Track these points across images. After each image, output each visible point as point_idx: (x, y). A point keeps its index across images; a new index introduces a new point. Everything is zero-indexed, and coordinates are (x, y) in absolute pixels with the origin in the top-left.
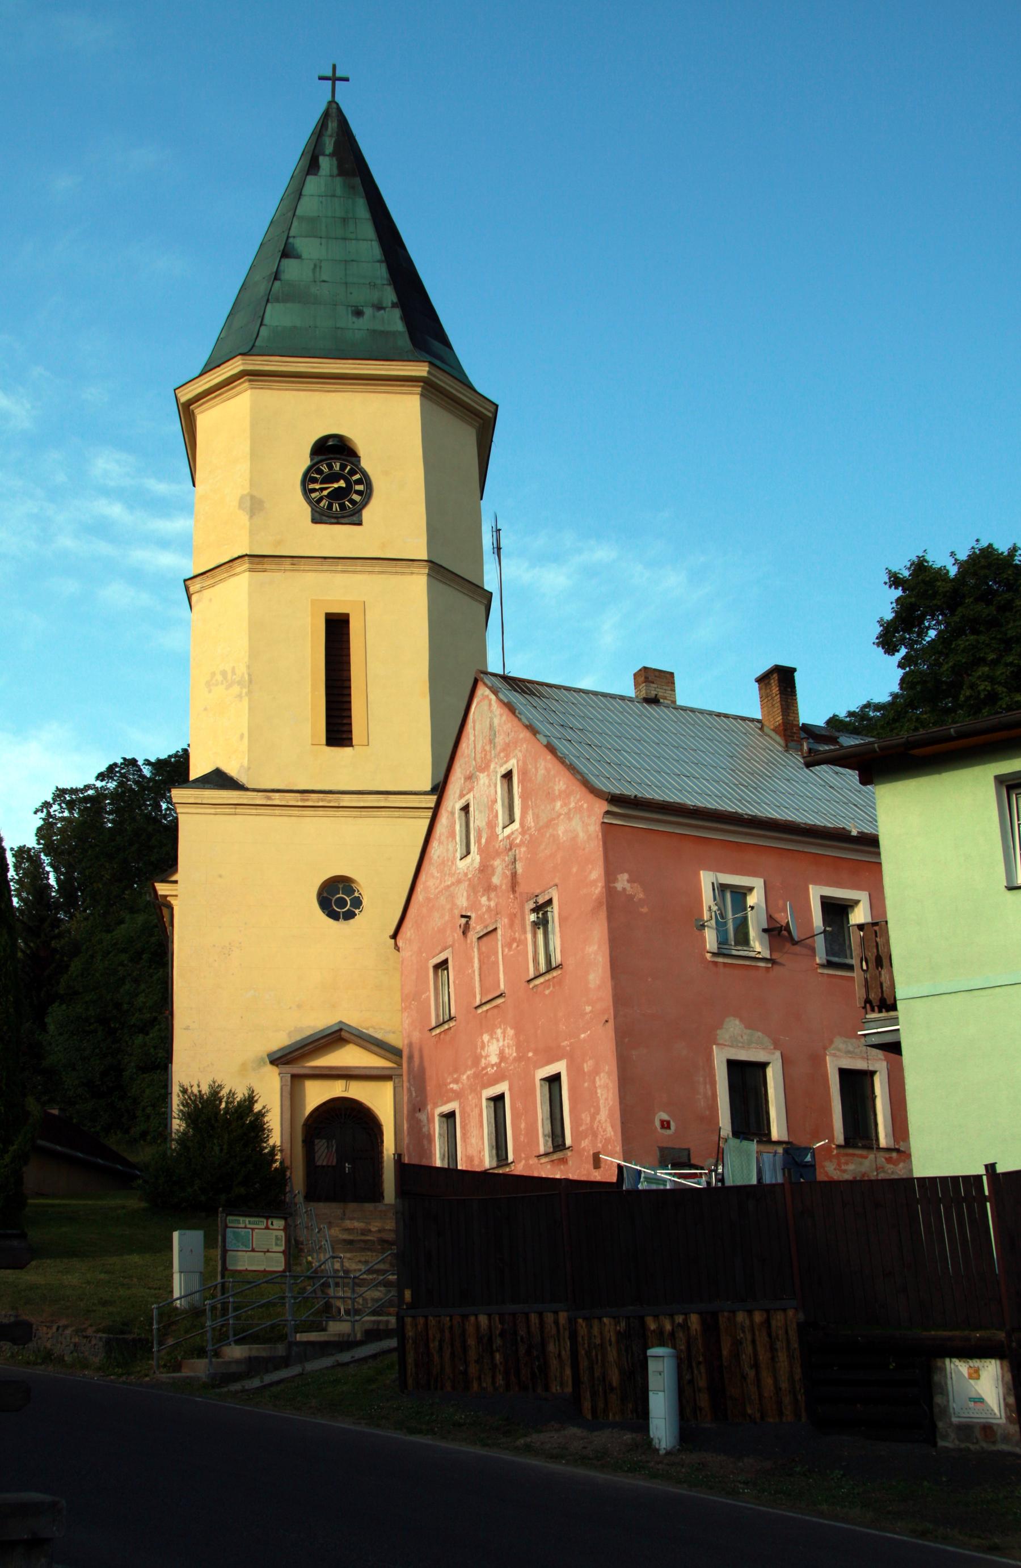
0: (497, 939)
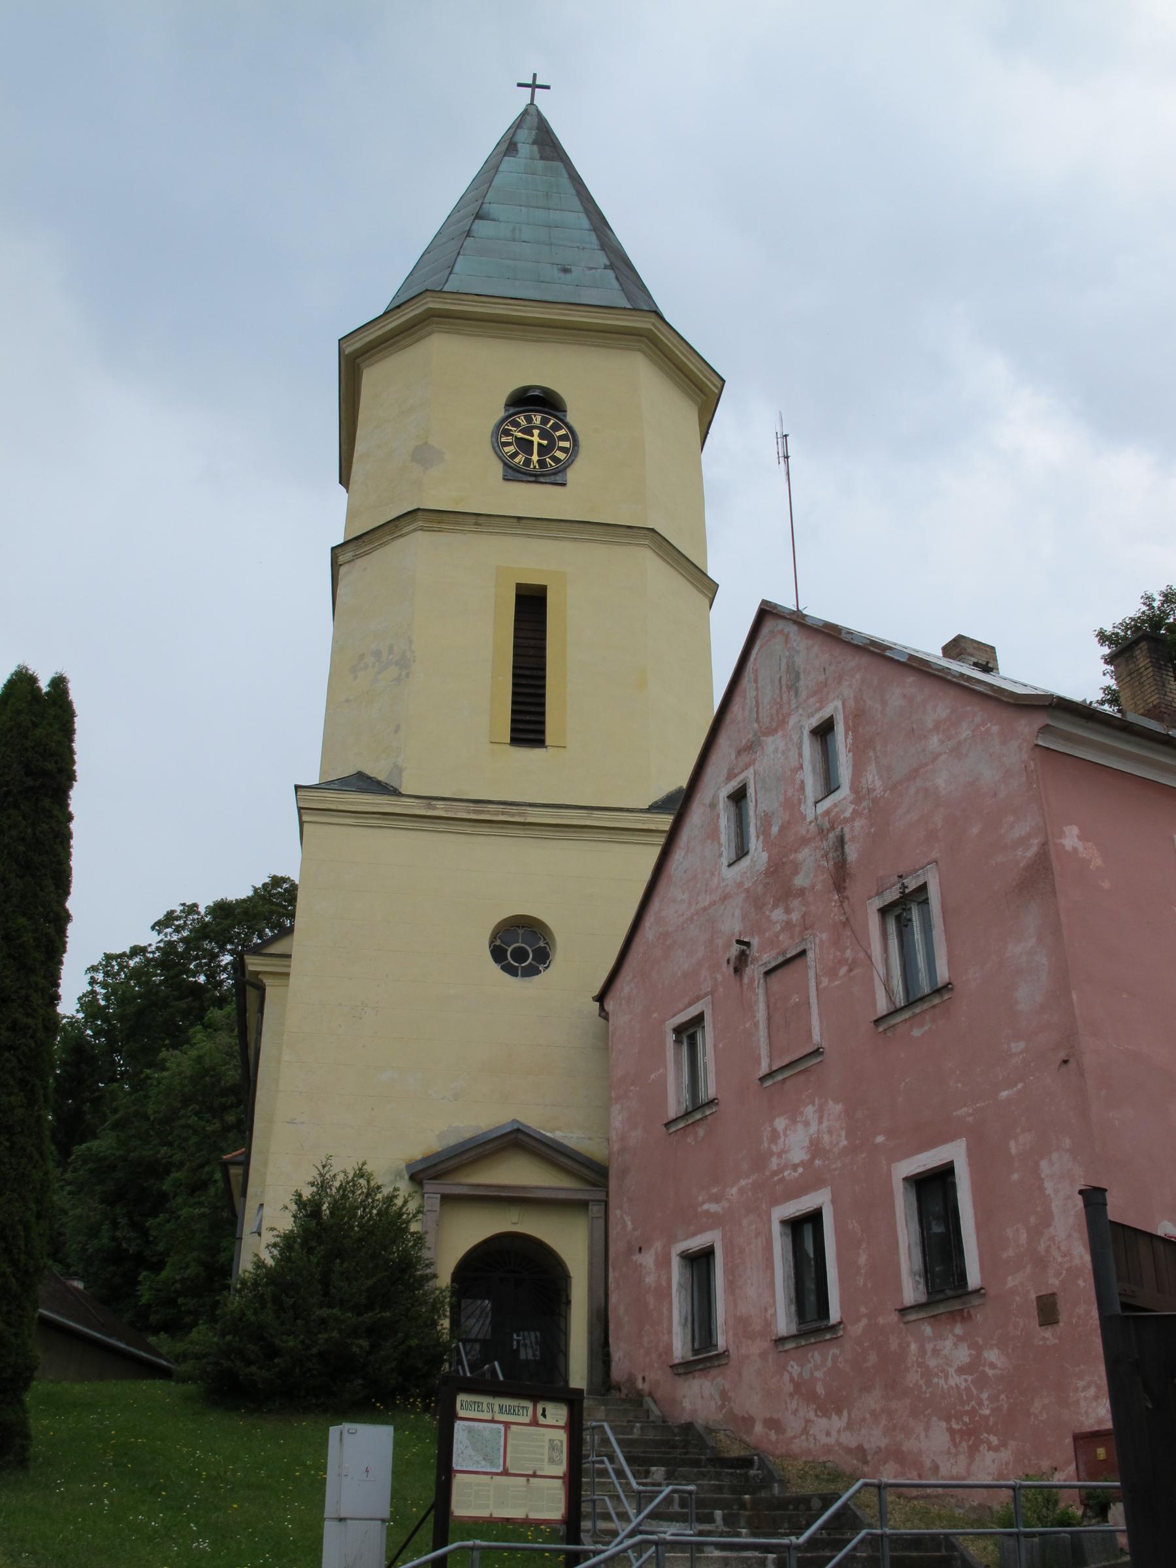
0: (807, 967)
